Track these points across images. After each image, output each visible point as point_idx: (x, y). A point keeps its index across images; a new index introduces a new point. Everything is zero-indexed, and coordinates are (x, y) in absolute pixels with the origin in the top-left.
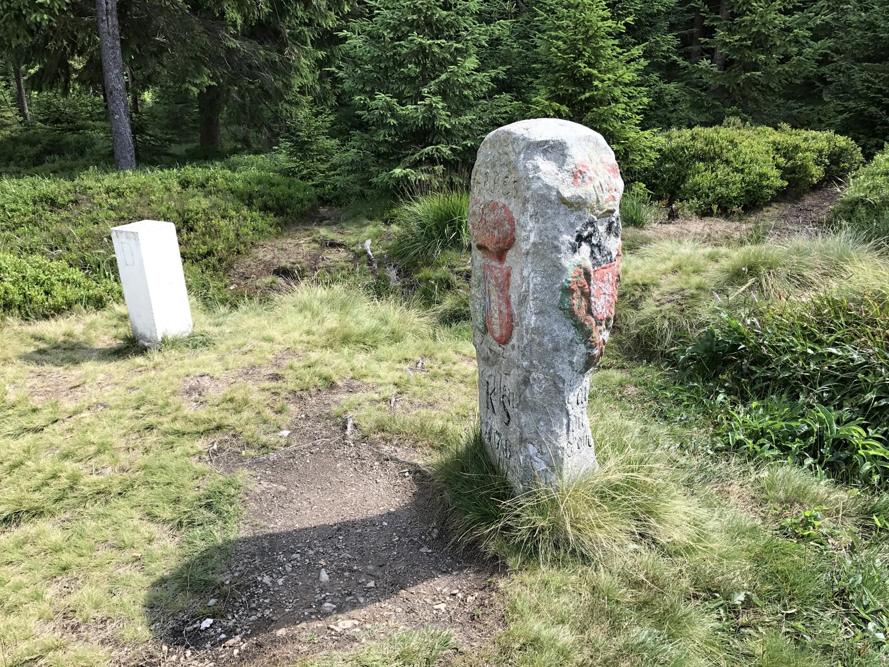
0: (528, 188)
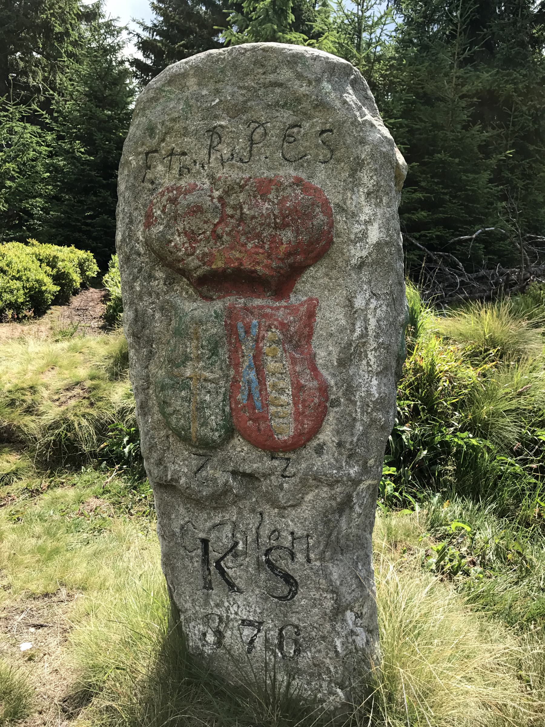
0: (363, 142)
